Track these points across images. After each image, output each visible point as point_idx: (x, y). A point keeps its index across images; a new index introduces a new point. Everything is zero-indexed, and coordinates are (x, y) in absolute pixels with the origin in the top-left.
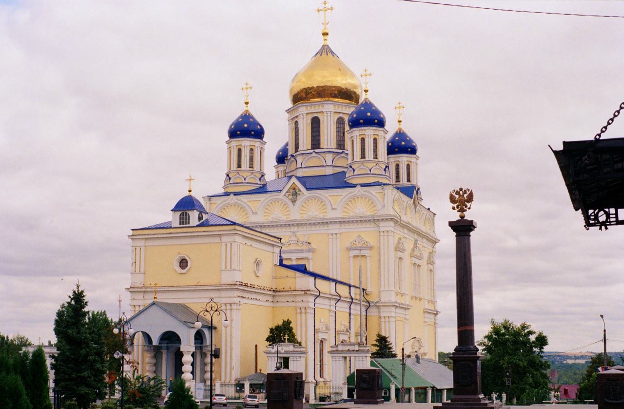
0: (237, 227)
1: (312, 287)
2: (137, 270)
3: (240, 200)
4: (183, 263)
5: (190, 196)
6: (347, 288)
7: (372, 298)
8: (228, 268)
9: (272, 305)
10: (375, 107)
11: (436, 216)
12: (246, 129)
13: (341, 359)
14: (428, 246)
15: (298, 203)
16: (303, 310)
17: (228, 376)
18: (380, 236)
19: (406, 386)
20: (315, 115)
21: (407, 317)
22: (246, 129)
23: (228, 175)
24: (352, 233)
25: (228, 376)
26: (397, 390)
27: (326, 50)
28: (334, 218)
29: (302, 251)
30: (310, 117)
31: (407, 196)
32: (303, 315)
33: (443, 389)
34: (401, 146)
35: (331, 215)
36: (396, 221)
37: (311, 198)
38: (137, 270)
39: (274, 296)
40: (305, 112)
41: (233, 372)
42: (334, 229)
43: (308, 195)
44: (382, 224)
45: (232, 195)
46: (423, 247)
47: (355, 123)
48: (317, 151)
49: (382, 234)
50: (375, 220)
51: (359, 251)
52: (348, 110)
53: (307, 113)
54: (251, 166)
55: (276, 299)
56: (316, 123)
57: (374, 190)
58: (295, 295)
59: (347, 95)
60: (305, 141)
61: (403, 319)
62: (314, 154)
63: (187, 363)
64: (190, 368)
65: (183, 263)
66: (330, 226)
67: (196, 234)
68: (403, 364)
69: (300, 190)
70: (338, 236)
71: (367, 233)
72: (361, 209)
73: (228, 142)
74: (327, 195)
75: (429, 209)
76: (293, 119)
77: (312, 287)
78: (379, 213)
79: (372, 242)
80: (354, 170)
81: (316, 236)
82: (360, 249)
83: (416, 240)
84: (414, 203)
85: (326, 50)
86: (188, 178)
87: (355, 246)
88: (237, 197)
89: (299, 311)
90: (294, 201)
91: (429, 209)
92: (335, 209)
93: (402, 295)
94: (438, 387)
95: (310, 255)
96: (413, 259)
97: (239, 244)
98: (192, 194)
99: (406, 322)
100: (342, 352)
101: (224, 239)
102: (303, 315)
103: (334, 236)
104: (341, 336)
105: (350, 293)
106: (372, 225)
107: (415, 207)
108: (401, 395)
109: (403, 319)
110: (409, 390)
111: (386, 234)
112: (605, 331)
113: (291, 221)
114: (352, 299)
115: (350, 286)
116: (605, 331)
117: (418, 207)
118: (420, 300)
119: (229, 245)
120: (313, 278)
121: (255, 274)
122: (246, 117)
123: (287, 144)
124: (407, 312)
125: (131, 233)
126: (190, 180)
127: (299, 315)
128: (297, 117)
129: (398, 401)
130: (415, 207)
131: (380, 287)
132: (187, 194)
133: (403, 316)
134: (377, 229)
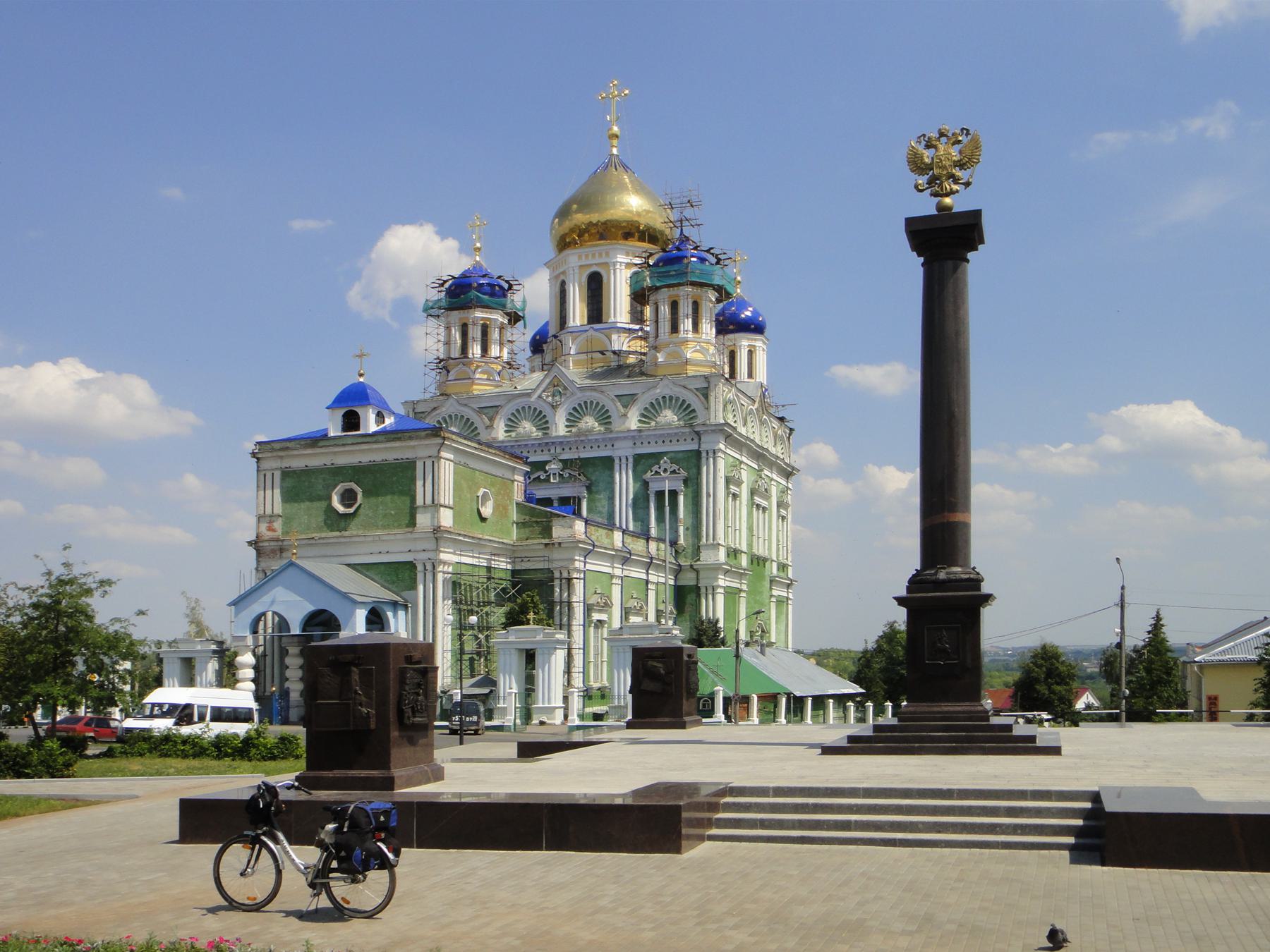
8: (429, 501)
19: (743, 692)
26: (727, 701)
31: (553, 805)
40: (578, 262)
56: (596, 287)
60: (578, 313)
63: (244, 666)
64: (288, 673)
67: (811, 801)
68: (737, 656)
86: (358, 352)
94: (798, 694)
108: (736, 705)
110: (746, 700)
112: (1123, 588)
116: (1123, 588)
119: (429, 463)
123: (547, 323)
128: (564, 273)
129: (728, 718)
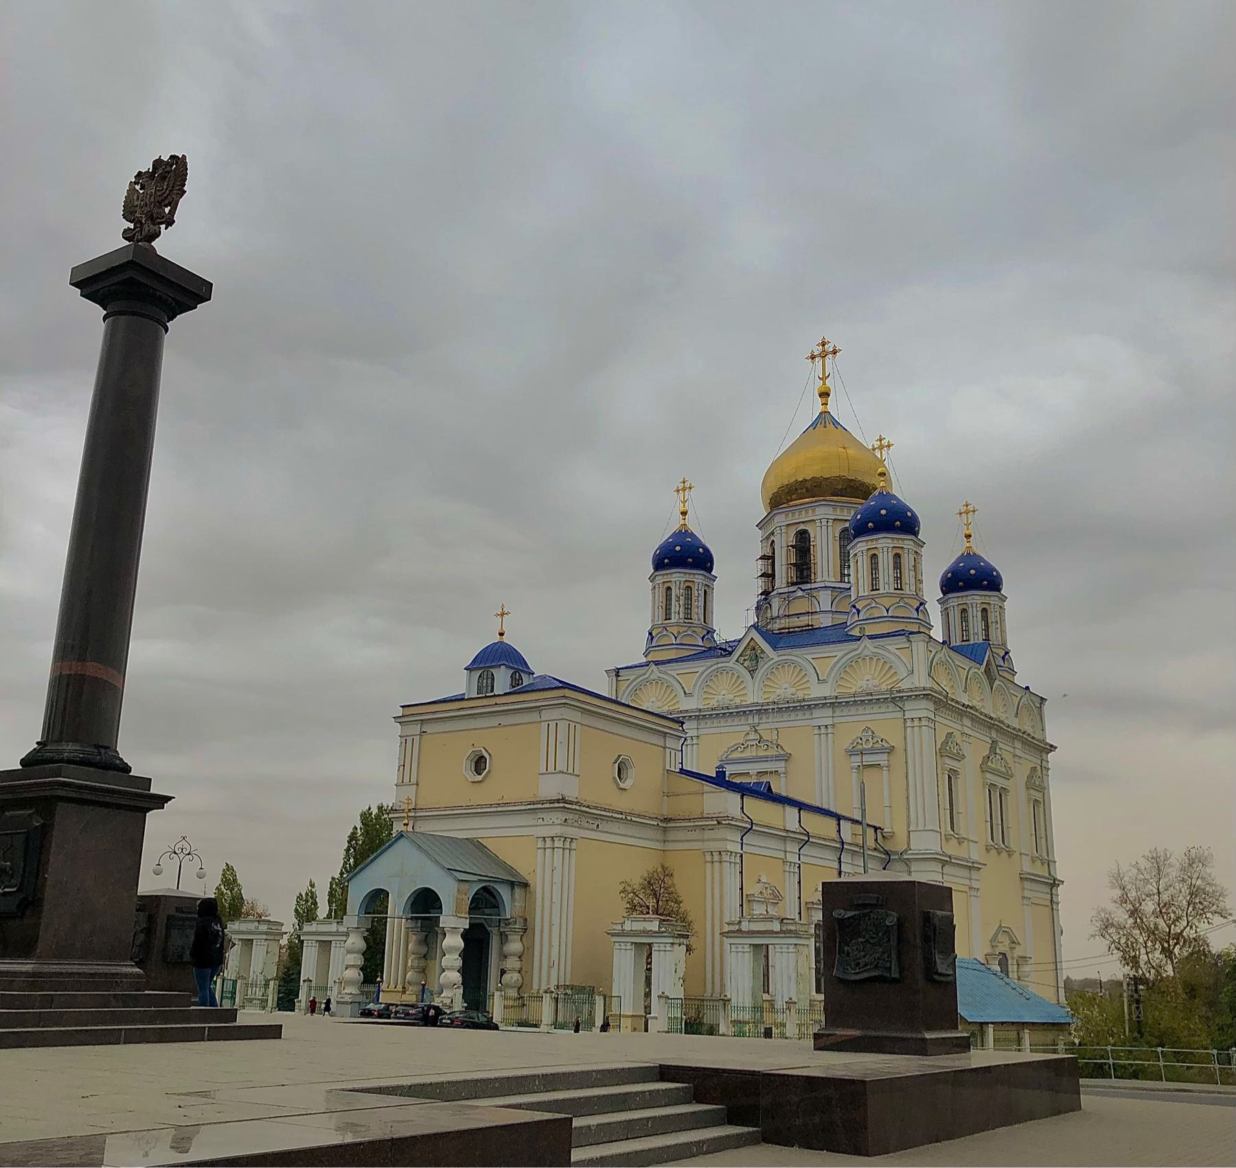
0: (567, 692)
1: (737, 813)
2: (406, 780)
3: (665, 673)
4: (479, 763)
5: (502, 642)
6: (834, 822)
7: (898, 845)
8: (551, 769)
9: (659, 846)
10: (984, 561)
11: (1046, 707)
12: (684, 556)
13: (747, 948)
14: (1032, 760)
15: (760, 674)
16: (716, 858)
17: (544, 979)
18: (905, 728)
20: (802, 527)
21: (975, 884)
22: (684, 556)
23: (650, 634)
24: (852, 726)
25: (544, 979)
27: (824, 419)
28: (819, 698)
29: (765, 759)
30: (793, 532)
32: (717, 865)
33: (987, 1023)
34: (971, 578)
35: (817, 691)
36: (941, 702)
37: (781, 664)
38: (406, 780)
39: (665, 830)
41: (554, 972)
42: (824, 717)
43: (777, 659)
44: (908, 705)
45: (653, 666)
46: (1015, 756)
47: (861, 529)
48: (804, 587)
49: (909, 724)
50: (896, 699)
51: (868, 756)
52: (849, 512)
53: (788, 525)
54: (688, 616)
55: (672, 836)
57: (893, 645)
58: (703, 828)
59: (853, 489)
61: (966, 889)
62: (800, 593)
65: (479, 763)
66: (817, 713)
69: (763, 652)
70: (830, 730)
71: (886, 725)
72: (866, 679)
73: (652, 579)
74: (809, 657)
75: (1027, 688)
76: (768, 538)
77: (737, 813)
78: (904, 685)
79: (894, 740)
80: (858, 611)
81: (795, 734)
82: (873, 751)
83: (994, 742)
84: (988, 671)
85: (824, 419)
87: (859, 747)
88: (661, 667)
89: (709, 858)
90: (752, 672)
91: (1027, 688)
92: (824, 681)
93: (960, 841)
95: (780, 766)
96: (988, 775)
97: (572, 725)
98: (505, 639)
99: (973, 893)
100: (752, 933)
101: (546, 715)
102: (717, 865)
103: (823, 730)
104: (755, 906)
105: (839, 831)
106: (891, 707)
107: (991, 681)
109: (966, 889)
111: (916, 723)
113: (747, 706)
114: (843, 843)
115: (839, 818)
117: (997, 682)
118: (1010, 856)
120: (738, 796)
121: (618, 785)
122: (683, 535)
124: (974, 874)
125: (400, 712)
126: (502, 615)
127: (709, 865)
128: (773, 533)
130: (991, 681)
131: (909, 826)
132: (497, 639)
133: (967, 882)
134: (900, 715)
